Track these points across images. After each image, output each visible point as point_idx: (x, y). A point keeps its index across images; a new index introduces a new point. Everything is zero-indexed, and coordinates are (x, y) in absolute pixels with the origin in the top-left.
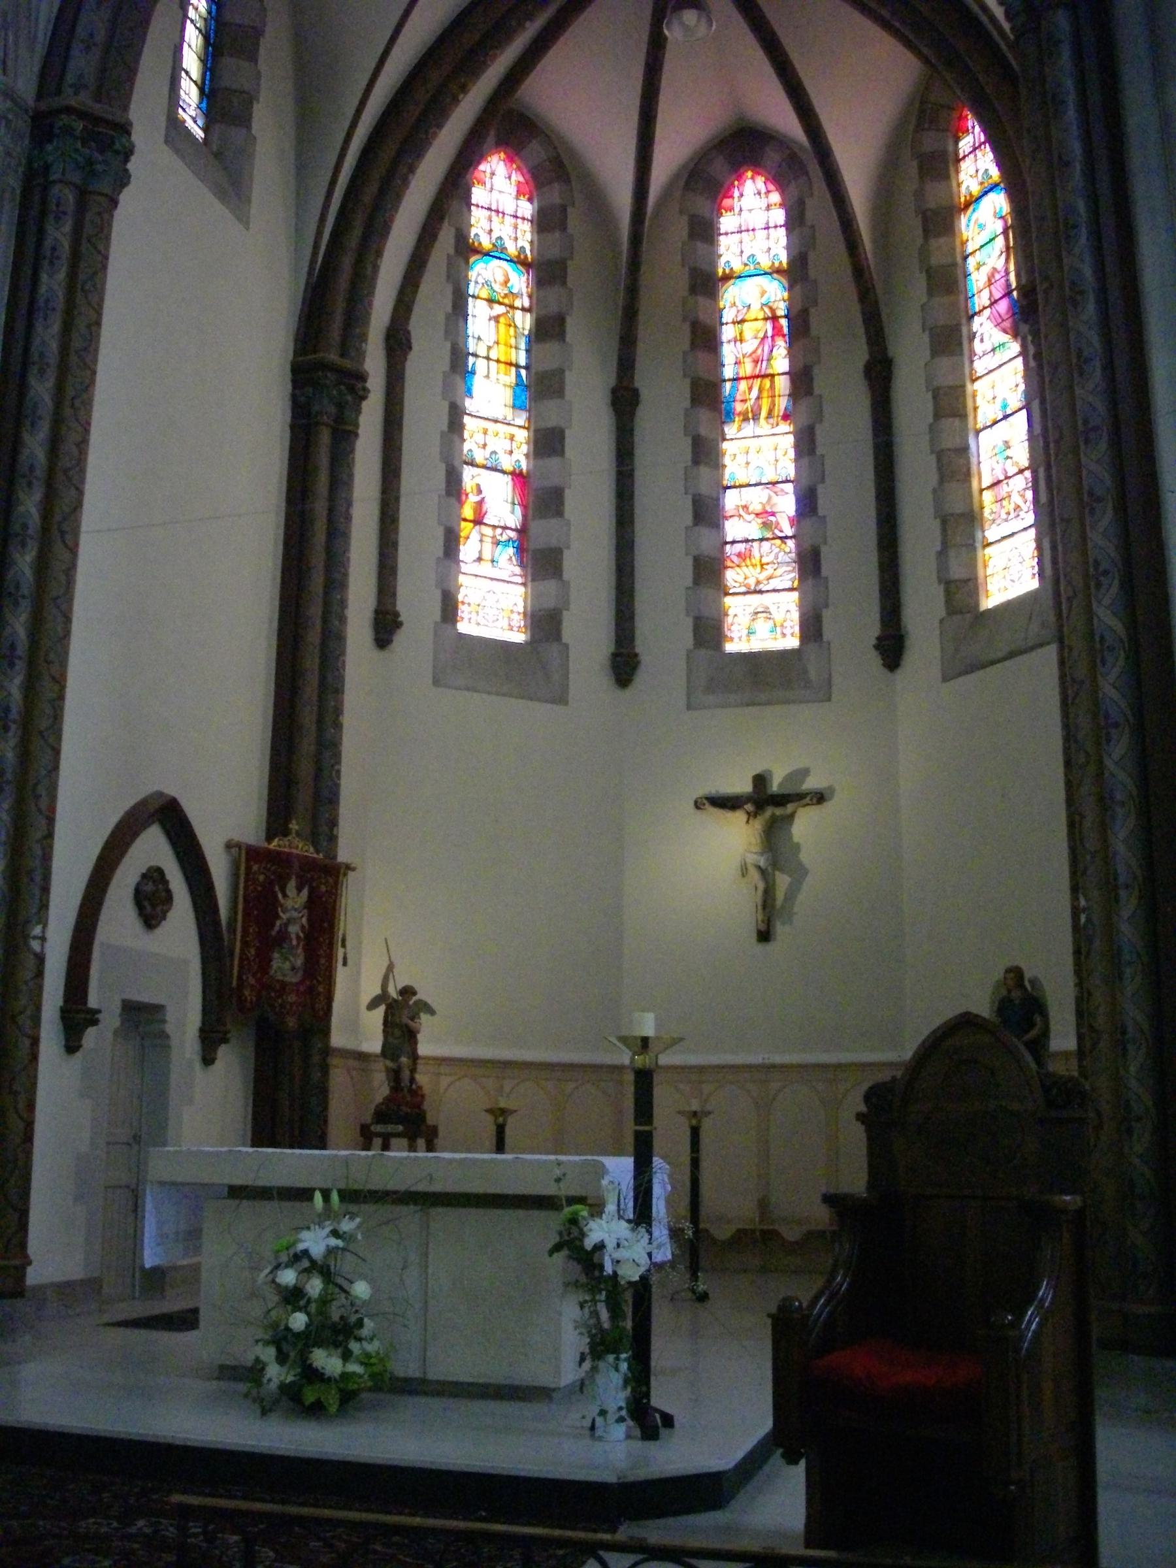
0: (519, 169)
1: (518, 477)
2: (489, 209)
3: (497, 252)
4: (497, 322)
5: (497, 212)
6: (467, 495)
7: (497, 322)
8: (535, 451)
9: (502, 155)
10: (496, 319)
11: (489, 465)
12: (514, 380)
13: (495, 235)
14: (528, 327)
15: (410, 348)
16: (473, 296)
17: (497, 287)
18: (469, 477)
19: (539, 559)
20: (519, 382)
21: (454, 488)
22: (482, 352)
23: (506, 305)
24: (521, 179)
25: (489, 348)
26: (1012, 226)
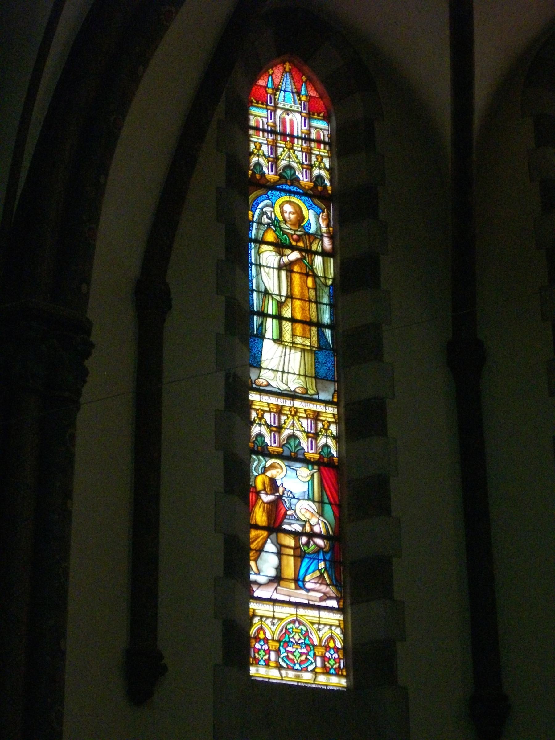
0: (309, 81)
1: (323, 464)
2: (273, 132)
3: (286, 182)
4: (290, 272)
5: (284, 135)
6: (258, 493)
7: (290, 272)
8: (347, 430)
9: (288, 66)
10: (288, 268)
11: (287, 453)
12: (315, 343)
13: (282, 163)
14: (331, 273)
15: (170, 307)
16: (256, 241)
17: (286, 227)
18: (261, 472)
19: (356, 567)
20: (322, 346)
21: (239, 486)
22: (271, 308)
23: (300, 250)
24: (313, 93)
25: (280, 305)
26: (337, 391)
